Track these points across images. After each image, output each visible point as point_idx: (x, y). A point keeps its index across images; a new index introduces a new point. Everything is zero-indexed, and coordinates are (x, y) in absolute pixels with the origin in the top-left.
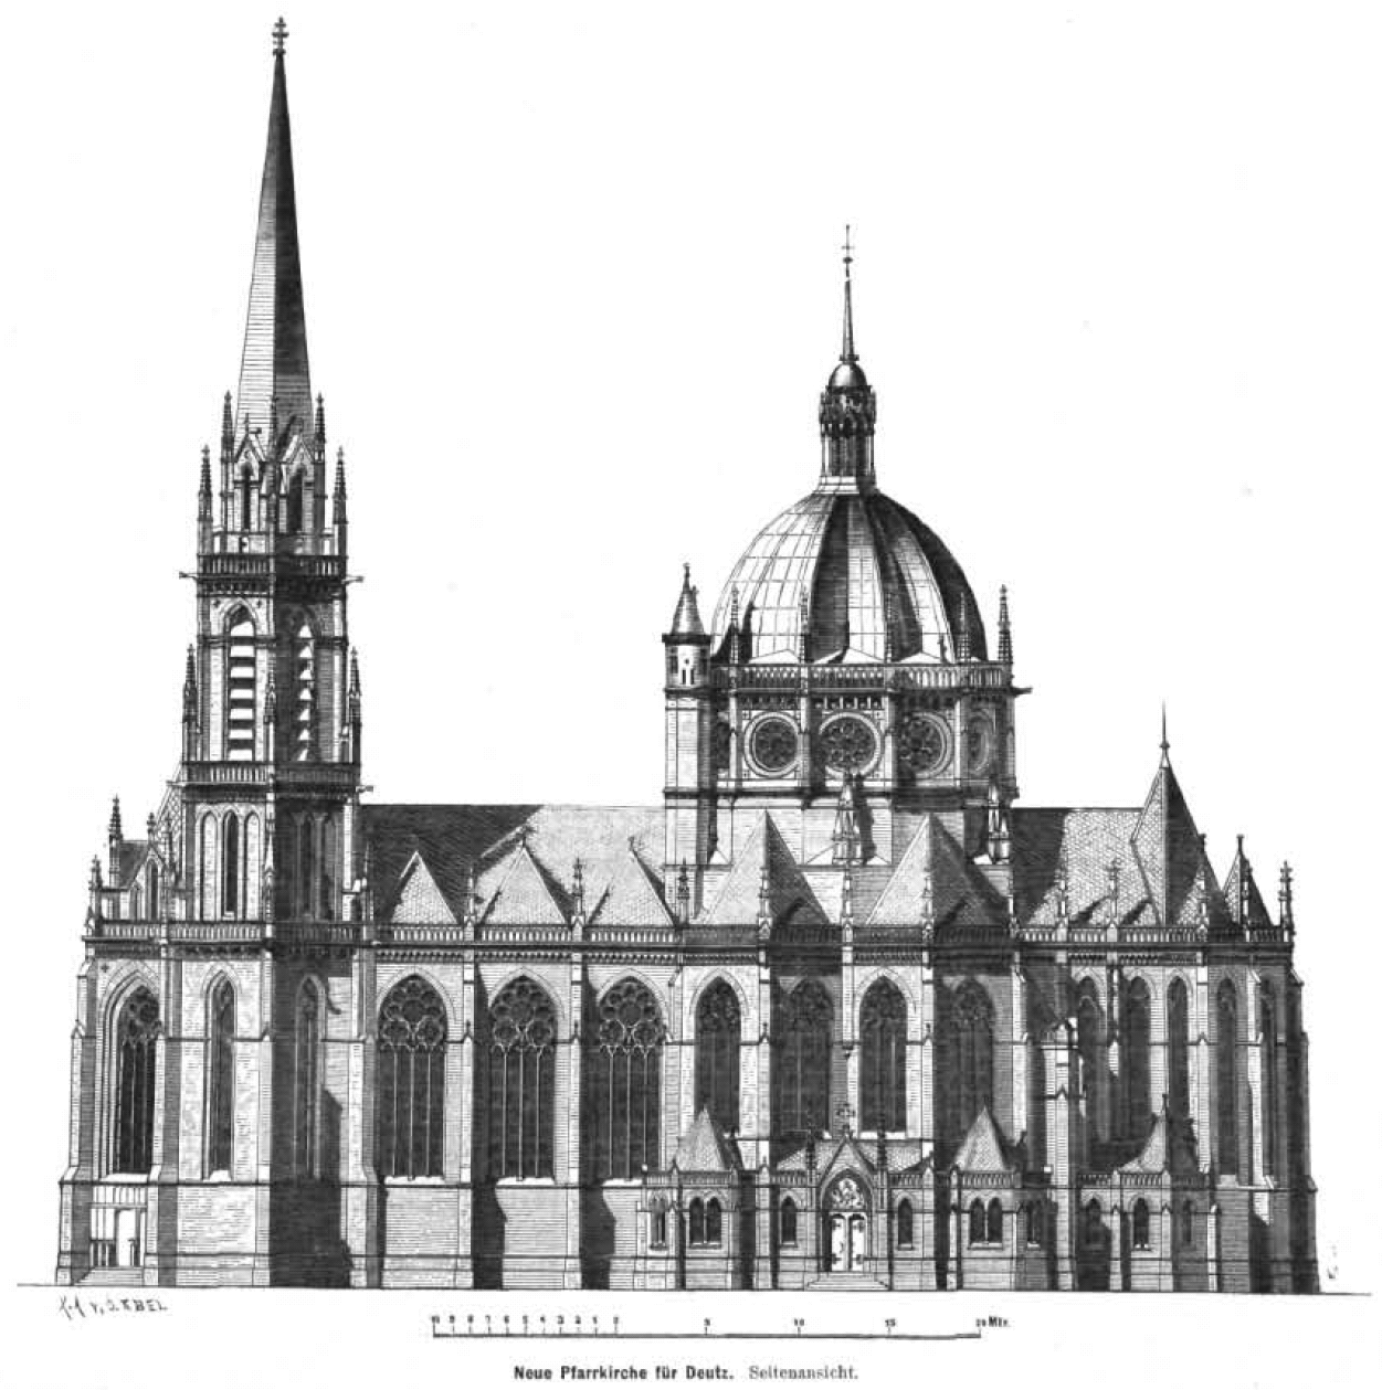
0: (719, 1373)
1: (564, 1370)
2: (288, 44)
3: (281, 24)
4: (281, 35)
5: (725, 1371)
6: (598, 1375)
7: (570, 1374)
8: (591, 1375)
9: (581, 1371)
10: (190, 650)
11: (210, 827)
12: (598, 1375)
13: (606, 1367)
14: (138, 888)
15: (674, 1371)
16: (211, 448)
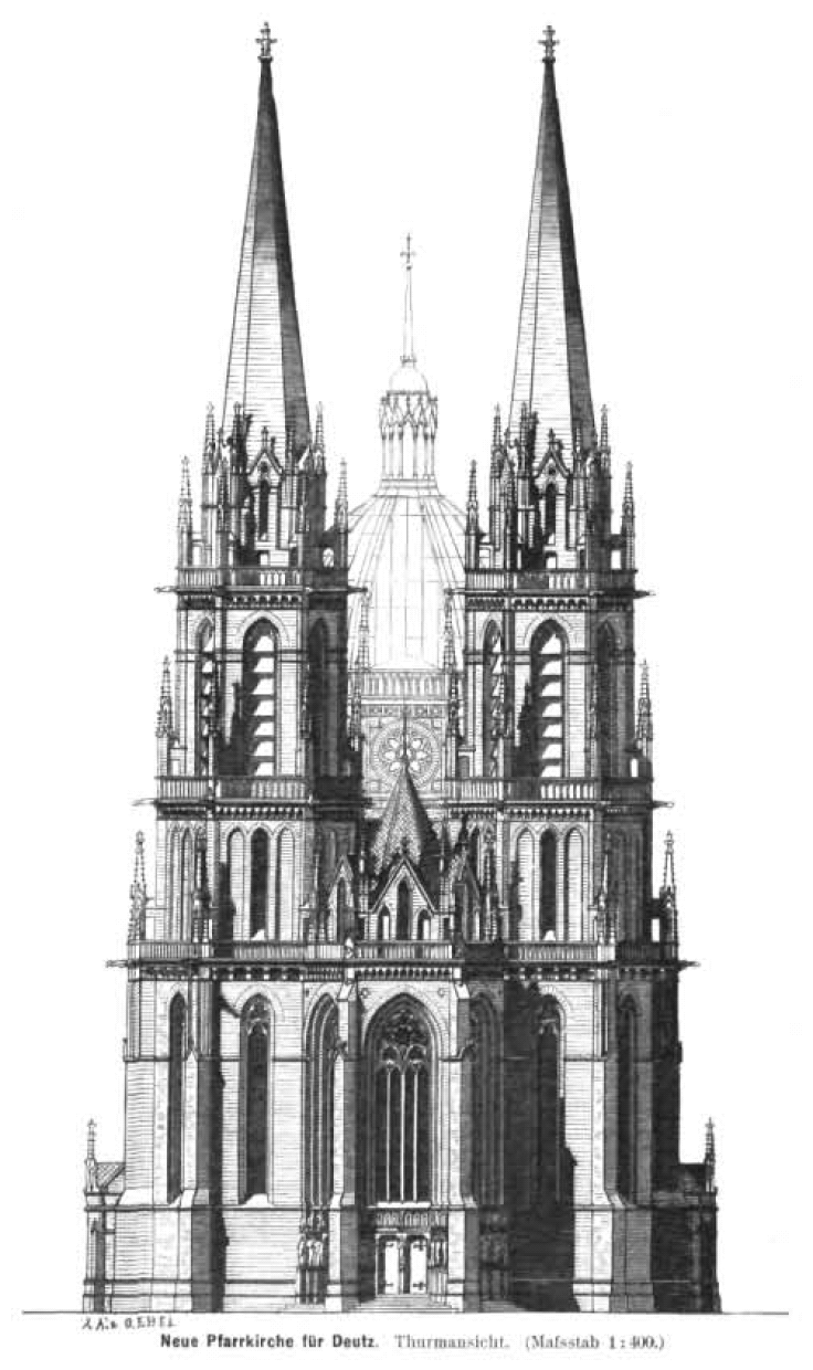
0: (366, 1342)
1: (211, 1339)
2: (558, 52)
3: (550, 31)
4: (549, 44)
5: (371, 1340)
6: (245, 1343)
7: (217, 1341)
8: (238, 1343)
9: (228, 1340)
10: (166, 662)
11: (237, 841)
12: (245, 1343)
13: (252, 1336)
14: (385, 912)
15: (320, 1340)
16: (191, 458)
